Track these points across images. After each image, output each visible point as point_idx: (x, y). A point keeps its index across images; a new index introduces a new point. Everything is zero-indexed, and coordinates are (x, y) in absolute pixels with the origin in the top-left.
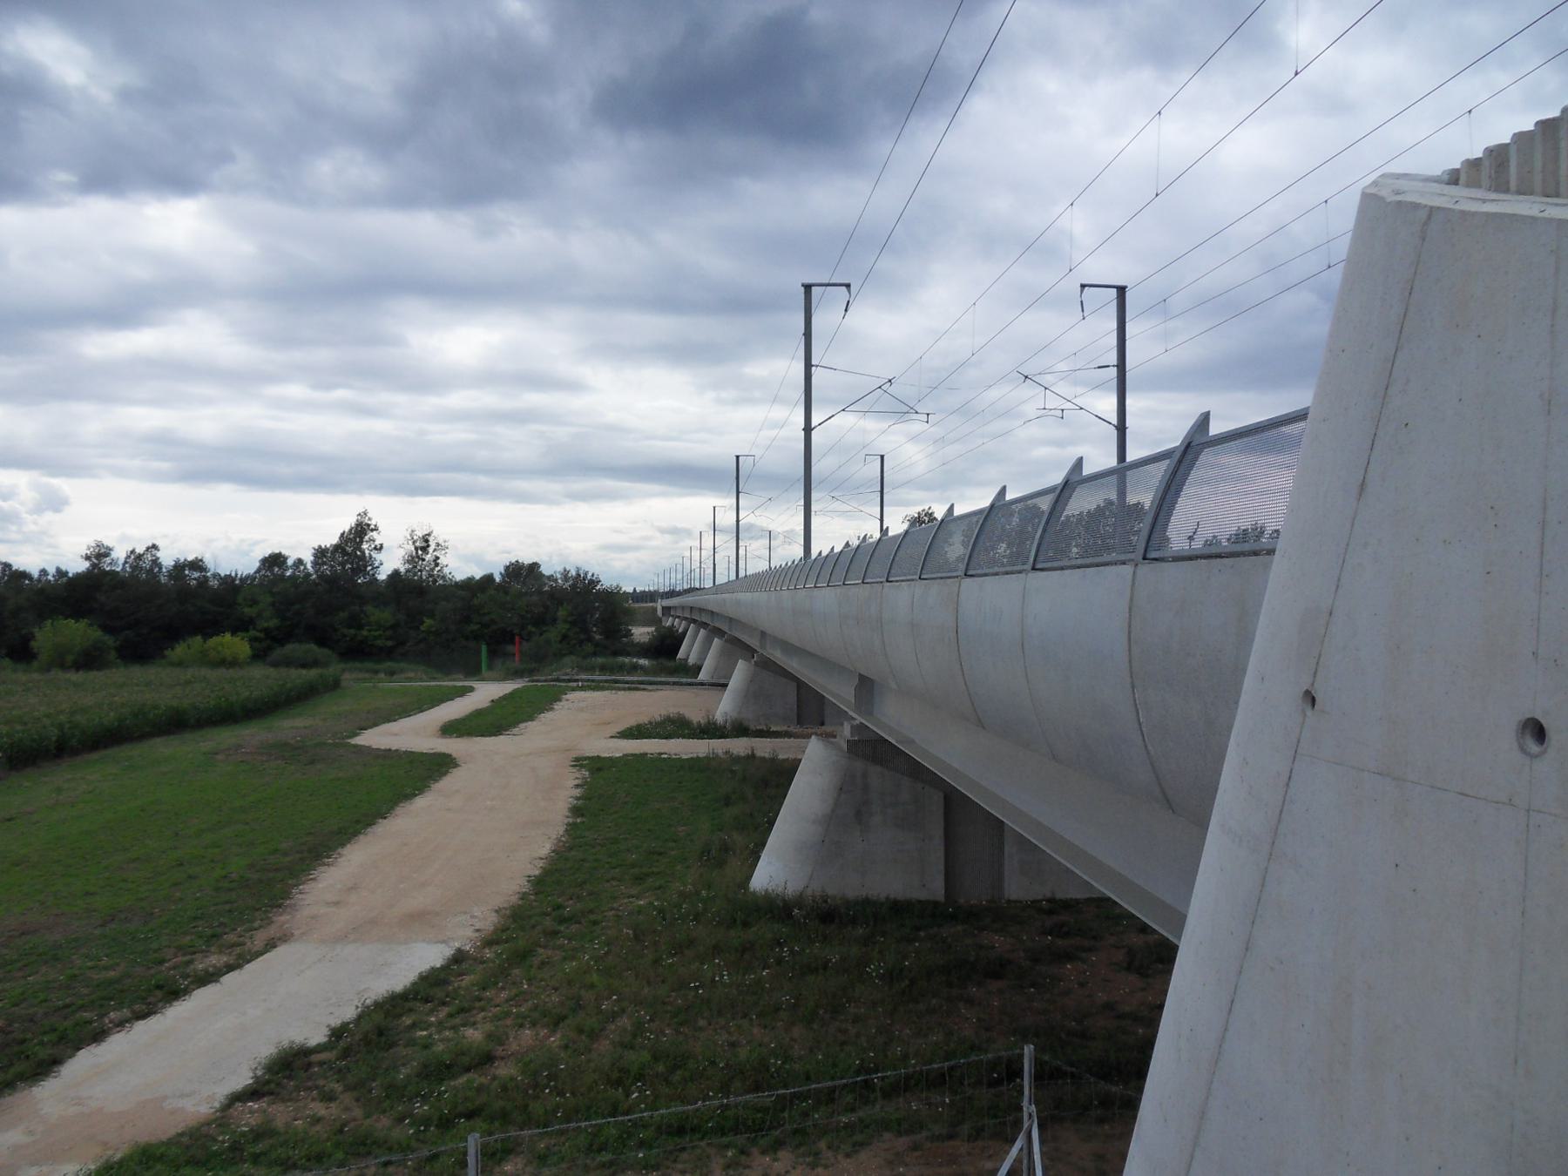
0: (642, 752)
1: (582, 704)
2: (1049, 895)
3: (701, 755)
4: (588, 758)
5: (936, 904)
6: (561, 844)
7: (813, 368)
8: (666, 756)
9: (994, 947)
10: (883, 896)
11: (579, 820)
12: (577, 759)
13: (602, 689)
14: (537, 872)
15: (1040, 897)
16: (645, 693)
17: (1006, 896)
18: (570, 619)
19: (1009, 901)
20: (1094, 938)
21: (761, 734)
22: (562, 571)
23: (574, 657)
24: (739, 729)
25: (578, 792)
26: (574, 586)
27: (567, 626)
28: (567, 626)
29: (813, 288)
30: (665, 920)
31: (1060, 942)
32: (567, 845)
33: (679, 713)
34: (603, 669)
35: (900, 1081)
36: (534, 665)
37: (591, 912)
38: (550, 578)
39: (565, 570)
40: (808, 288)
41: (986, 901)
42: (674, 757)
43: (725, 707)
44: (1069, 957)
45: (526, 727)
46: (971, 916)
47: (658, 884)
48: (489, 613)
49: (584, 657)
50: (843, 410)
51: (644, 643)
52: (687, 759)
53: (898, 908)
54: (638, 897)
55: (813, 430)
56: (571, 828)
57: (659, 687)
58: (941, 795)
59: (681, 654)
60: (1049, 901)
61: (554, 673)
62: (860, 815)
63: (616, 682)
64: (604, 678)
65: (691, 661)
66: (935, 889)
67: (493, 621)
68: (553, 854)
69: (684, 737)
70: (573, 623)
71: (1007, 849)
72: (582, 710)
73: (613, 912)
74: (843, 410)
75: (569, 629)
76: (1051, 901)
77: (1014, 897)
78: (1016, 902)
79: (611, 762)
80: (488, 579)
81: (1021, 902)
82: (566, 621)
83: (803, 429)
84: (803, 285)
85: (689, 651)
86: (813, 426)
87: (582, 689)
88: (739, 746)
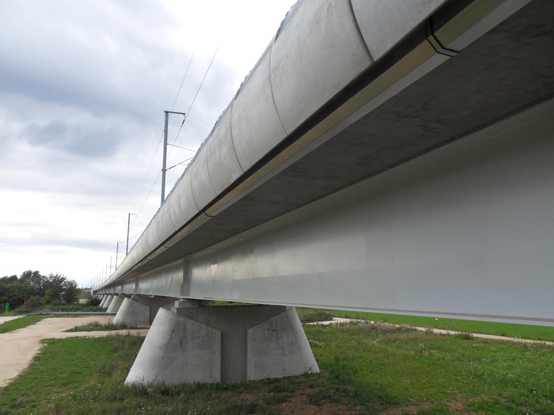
0: (76, 336)
1: (50, 322)
2: (267, 377)
3: (104, 336)
4: (47, 340)
5: (218, 384)
6: (24, 372)
7: (167, 145)
8: (87, 337)
9: (248, 399)
10: (192, 382)
11: (37, 363)
12: (42, 340)
13: (62, 317)
14: (6, 385)
15: (263, 378)
16: (83, 318)
17: (248, 379)
18: (51, 294)
19: (250, 381)
20: (292, 392)
21: (132, 328)
22: (50, 274)
23: (49, 305)
24: (123, 326)
25: (39, 352)
26: (54, 281)
27: (49, 297)
28: (49, 297)
29: (169, 113)
30: (76, 400)
31: (276, 394)
32: (27, 373)
33: (96, 322)
34: (63, 310)
35: (551, 413)
36: (30, 309)
37: (33, 401)
38: (44, 277)
39: (51, 274)
40: (167, 113)
41: (240, 382)
42: (91, 337)
43: (117, 319)
44: (284, 400)
45: (20, 330)
46: (234, 388)
47: (75, 385)
48: (12, 292)
49: (55, 305)
50: (180, 164)
51: (84, 304)
52: (98, 338)
53: (200, 387)
54: (62, 392)
55: (166, 170)
56: (32, 366)
57: (88, 316)
58: (220, 332)
59: (101, 305)
60: (267, 379)
61: (39, 312)
62: (182, 343)
63: (68, 314)
64: (63, 313)
65: (104, 306)
66: (217, 377)
67: (14, 295)
68: (18, 377)
69: (97, 330)
70: (52, 296)
71: (249, 357)
72: (50, 324)
73: (47, 400)
74: (180, 164)
75: (50, 298)
76: (268, 379)
77: (251, 379)
78: (253, 381)
79: (60, 340)
80: (14, 278)
81: (255, 381)
82: (49, 295)
83: (164, 131)
84: (165, 112)
85: (104, 304)
86: (166, 169)
87: (51, 317)
88: (124, 332)
